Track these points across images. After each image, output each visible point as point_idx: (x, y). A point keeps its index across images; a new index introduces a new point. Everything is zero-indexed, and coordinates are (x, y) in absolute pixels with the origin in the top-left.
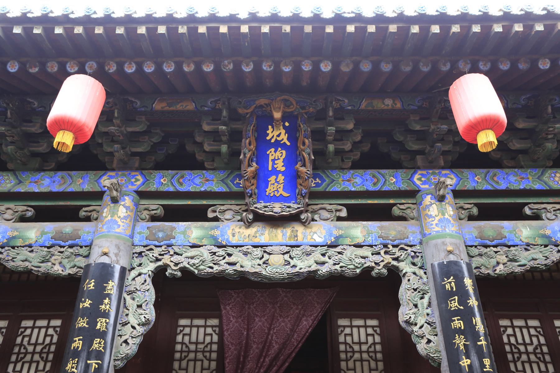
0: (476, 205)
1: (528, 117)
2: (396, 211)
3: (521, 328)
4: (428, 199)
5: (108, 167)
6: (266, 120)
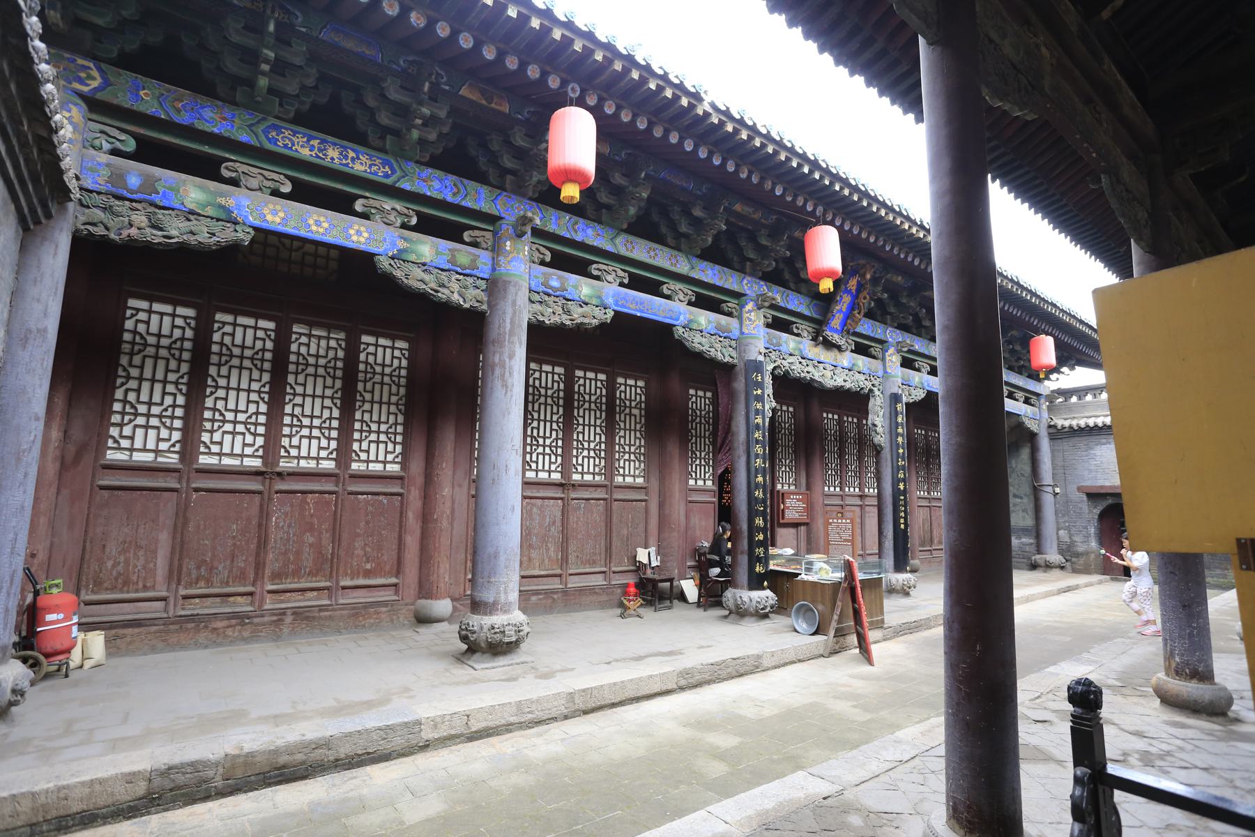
0: (418, 214)
2: (359, 206)
3: (547, 373)
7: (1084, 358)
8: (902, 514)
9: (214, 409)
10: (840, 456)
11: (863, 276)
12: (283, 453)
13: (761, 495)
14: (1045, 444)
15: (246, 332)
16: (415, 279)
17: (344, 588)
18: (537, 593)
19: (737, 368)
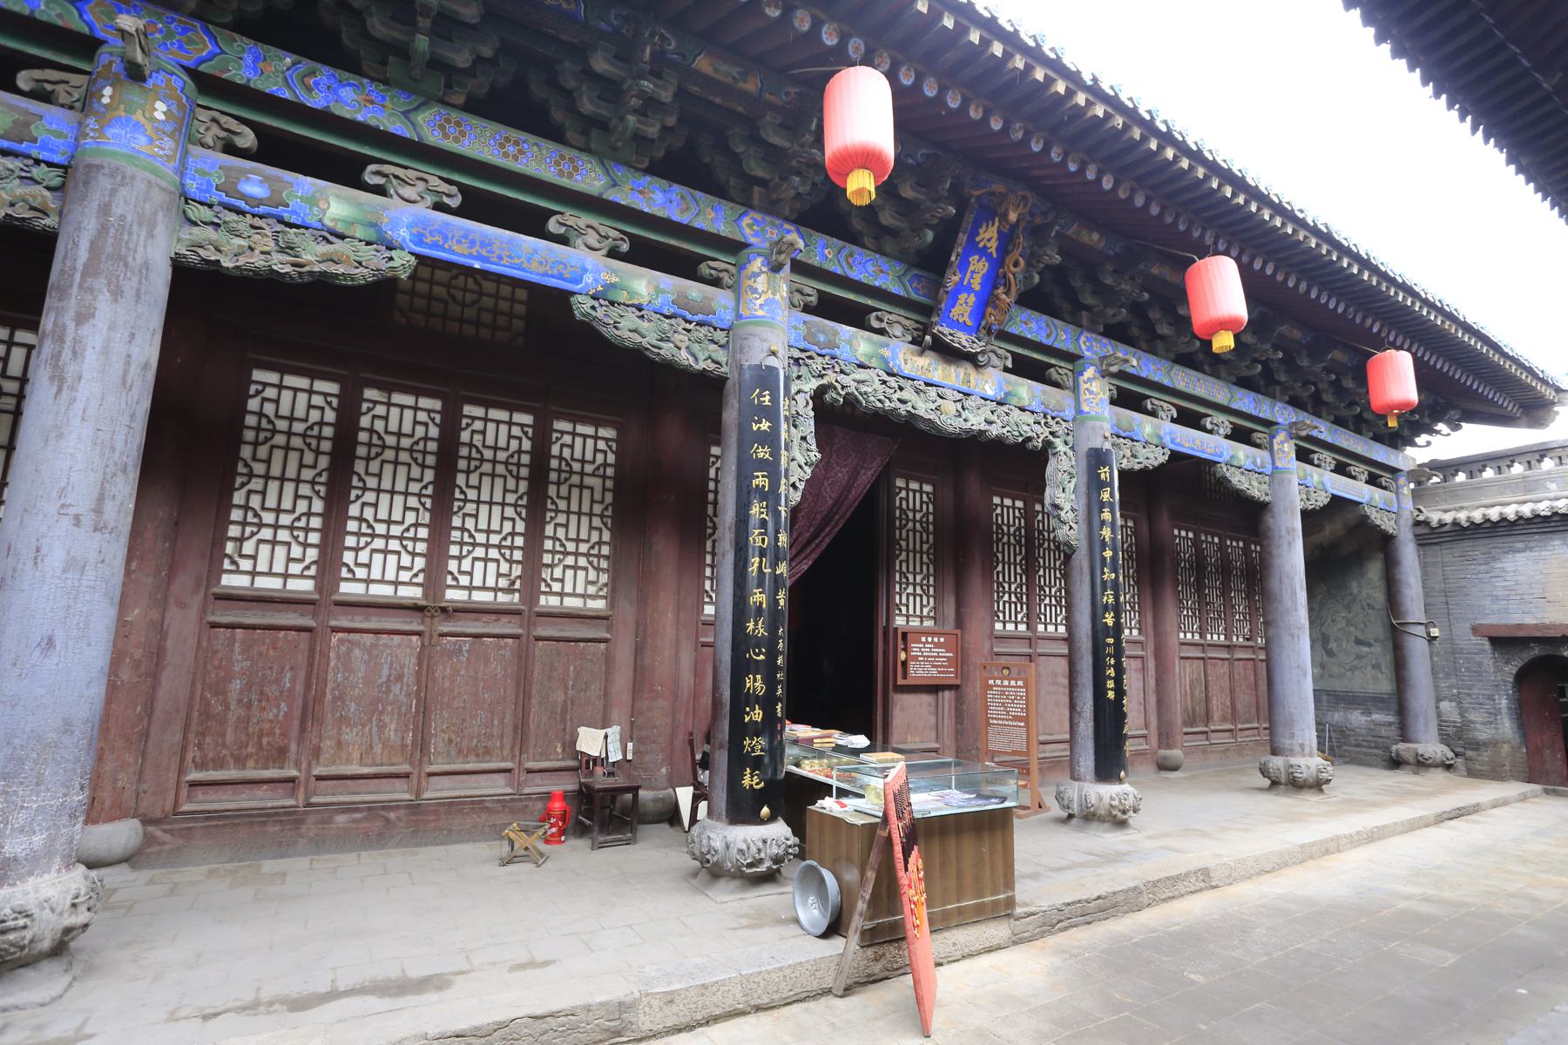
0: (463, 188)
1: (918, 184)
2: (553, 226)
3: (914, 492)
4: (757, 264)
5: (365, 68)
6: (989, 212)
7: (1478, 407)
8: (1111, 672)
9: (361, 519)
10: (1223, 594)
11: (1004, 217)
12: (449, 581)
13: (761, 631)
14: (1409, 554)
15: (402, 415)
16: (627, 328)
17: (529, 771)
18: (349, 808)
19: (729, 384)
